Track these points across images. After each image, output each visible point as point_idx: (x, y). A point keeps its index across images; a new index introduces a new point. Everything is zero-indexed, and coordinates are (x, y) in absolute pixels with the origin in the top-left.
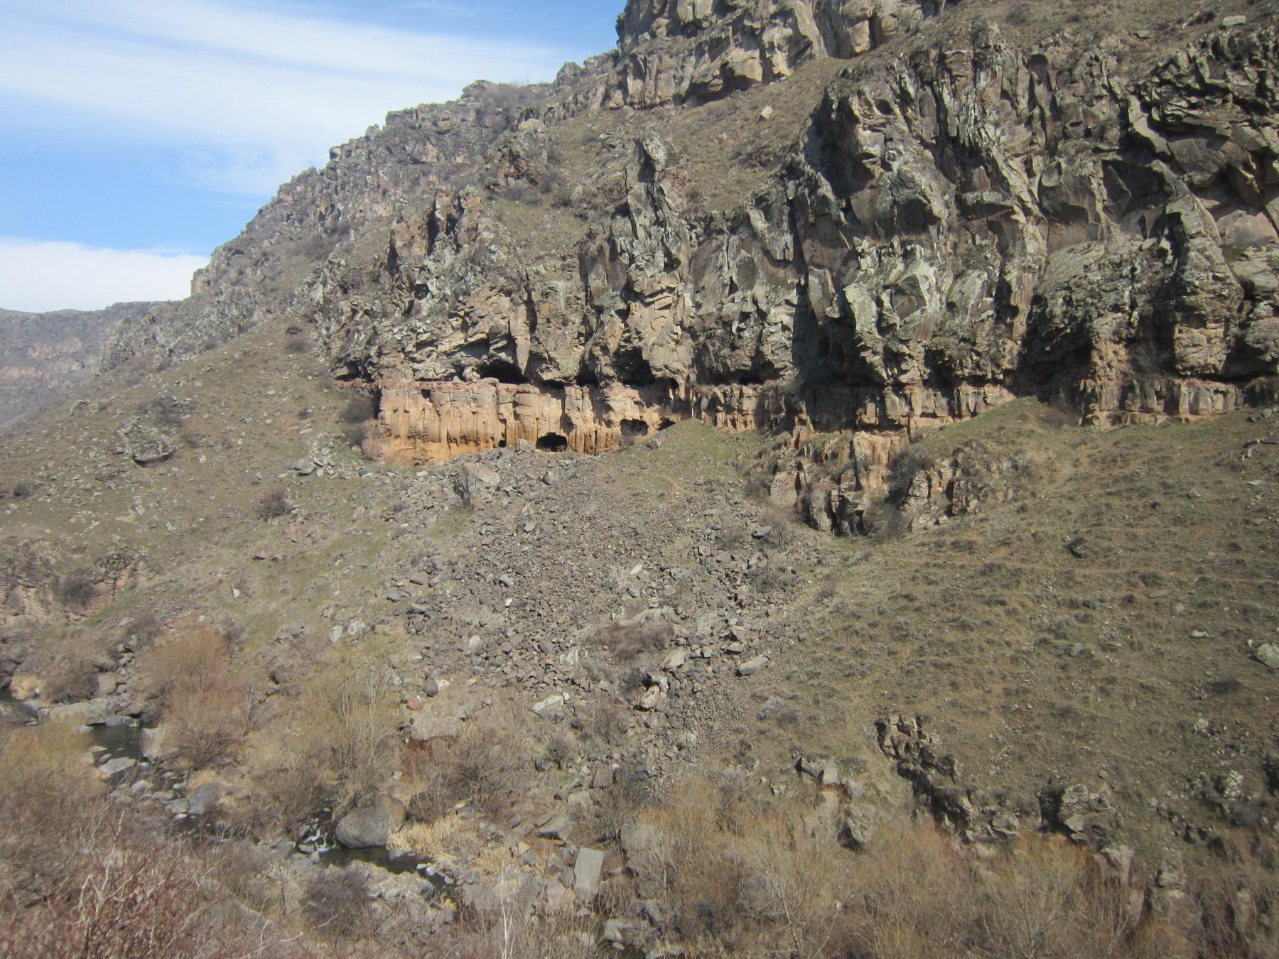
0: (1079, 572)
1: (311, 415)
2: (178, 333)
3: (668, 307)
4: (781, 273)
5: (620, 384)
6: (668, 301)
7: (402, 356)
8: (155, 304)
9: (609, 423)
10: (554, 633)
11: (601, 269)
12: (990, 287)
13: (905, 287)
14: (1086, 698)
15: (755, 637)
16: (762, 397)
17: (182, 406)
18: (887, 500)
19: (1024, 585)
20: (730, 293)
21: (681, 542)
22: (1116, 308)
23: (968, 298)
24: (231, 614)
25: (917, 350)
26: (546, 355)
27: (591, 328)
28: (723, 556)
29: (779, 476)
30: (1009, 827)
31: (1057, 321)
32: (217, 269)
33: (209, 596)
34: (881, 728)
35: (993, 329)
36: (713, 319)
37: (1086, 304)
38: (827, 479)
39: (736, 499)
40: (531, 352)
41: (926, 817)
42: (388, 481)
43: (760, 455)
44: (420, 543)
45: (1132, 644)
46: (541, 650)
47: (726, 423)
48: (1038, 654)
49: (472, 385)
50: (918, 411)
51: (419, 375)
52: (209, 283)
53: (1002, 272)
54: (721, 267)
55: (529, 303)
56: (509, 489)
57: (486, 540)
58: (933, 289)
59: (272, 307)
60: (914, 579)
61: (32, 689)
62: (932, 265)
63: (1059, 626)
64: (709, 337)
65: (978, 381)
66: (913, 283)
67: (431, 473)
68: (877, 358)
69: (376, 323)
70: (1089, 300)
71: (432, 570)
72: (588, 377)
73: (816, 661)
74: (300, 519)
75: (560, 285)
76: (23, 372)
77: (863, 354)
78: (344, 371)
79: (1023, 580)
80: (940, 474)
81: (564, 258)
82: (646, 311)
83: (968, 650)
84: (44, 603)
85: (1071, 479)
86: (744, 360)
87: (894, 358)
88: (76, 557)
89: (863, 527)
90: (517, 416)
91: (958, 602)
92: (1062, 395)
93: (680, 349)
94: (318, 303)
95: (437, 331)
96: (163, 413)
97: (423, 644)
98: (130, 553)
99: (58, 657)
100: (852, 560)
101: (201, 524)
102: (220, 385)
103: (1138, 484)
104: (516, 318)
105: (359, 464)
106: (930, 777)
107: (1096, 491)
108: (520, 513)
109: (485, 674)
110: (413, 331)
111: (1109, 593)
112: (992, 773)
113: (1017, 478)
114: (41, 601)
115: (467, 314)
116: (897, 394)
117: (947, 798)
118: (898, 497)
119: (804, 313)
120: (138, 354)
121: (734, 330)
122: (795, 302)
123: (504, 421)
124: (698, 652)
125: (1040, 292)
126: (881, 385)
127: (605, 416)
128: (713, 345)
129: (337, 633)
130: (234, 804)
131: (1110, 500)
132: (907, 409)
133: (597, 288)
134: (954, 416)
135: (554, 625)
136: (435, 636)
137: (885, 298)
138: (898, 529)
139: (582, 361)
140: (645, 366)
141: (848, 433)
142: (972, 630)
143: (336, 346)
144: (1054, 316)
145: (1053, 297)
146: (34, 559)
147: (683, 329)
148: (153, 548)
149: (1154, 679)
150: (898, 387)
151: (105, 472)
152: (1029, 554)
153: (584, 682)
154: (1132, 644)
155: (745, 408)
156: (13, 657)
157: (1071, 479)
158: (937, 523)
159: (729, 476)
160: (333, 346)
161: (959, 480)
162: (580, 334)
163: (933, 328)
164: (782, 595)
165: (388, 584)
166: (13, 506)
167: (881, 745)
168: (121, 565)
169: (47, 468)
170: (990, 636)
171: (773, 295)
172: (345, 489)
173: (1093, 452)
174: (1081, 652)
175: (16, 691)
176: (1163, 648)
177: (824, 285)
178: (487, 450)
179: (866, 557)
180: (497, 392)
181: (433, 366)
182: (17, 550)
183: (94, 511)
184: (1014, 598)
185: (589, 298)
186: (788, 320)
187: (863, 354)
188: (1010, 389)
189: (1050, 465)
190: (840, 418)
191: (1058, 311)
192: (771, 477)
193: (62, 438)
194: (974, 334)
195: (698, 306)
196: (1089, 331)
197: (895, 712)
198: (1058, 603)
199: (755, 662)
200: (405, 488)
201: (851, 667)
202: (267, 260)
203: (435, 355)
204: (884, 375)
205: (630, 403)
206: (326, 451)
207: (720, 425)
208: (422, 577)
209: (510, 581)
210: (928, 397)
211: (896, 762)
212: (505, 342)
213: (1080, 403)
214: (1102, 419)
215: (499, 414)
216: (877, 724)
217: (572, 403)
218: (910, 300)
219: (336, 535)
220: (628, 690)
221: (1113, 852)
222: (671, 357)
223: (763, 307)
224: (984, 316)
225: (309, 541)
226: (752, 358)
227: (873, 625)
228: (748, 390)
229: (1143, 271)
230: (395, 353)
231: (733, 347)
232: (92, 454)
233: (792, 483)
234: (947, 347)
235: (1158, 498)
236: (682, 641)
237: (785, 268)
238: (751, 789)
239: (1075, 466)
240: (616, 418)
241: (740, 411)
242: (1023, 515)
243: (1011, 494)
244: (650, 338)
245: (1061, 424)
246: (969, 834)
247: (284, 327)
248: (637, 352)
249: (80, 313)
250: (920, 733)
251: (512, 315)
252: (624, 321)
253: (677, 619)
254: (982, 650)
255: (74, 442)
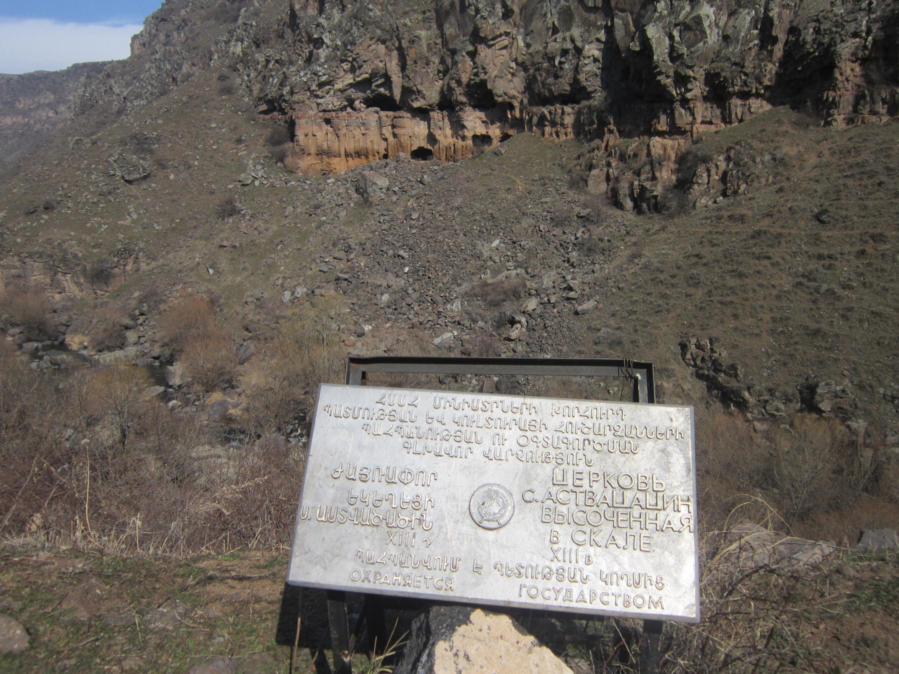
0: (824, 234)
1: (244, 141)
2: (128, 84)
3: (505, 47)
4: (592, 17)
5: (471, 108)
6: (506, 42)
7: (309, 94)
8: (110, 62)
9: (464, 138)
10: (441, 290)
11: (453, 20)
12: (757, 21)
13: (692, 24)
14: (832, 322)
15: (586, 288)
16: (578, 114)
17: (151, 139)
18: (675, 187)
19: (783, 244)
20: (553, 35)
21: (526, 222)
22: (855, 35)
23: (740, 31)
24: (210, 286)
25: (699, 73)
26: (415, 88)
27: (447, 66)
28: (557, 231)
29: (595, 172)
30: (778, 410)
31: (808, 46)
32: (150, 33)
33: (192, 274)
34: (684, 347)
35: (758, 55)
36: (540, 55)
37: (831, 32)
38: (630, 173)
39: (563, 190)
40: (403, 87)
41: (718, 406)
42: (307, 187)
43: (579, 157)
44: (337, 230)
45: (864, 284)
46: (433, 302)
47: (551, 134)
48: (796, 293)
49: (361, 114)
50: (699, 120)
51: (321, 108)
52: (144, 45)
53: (767, 9)
54: (545, 14)
55: (400, 49)
56: (396, 189)
57: (384, 227)
58: (713, 25)
59: (196, 62)
60: (701, 243)
61: (81, 343)
62: (712, 6)
63: (811, 273)
64: (538, 69)
65: (745, 96)
66: (698, 20)
67: (337, 180)
68: (669, 80)
69: (285, 69)
70: (834, 29)
71: (348, 250)
72: (447, 104)
73: (634, 303)
74: (248, 217)
75: (423, 33)
76: (15, 119)
77: (659, 78)
78: (264, 107)
79: (783, 241)
80: (717, 166)
81: (424, 13)
82: (489, 52)
83: (745, 291)
84: (78, 284)
85: (816, 167)
86: (564, 85)
87: (682, 80)
88: (95, 251)
89: (657, 207)
90: (395, 135)
91: (735, 259)
92: (809, 104)
93: (516, 80)
94: (239, 55)
95: (333, 74)
96: (138, 144)
97: (349, 301)
98: (132, 246)
99: (95, 321)
100: (653, 231)
101: (178, 224)
102: (175, 122)
103: (868, 169)
104: (391, 61)
105: (284, 176)
106: (720, 379)
107: (835, 175)
108: (406, 206)
109: (396, 320)
110: (315, 74)
111: (847, 248)
112: (765, 374)
113: (776, 167)
114: (76, 283)
115: (354, 59)
116: (683, 107)
117: (733, 392)
118: (684, 184)
119: (610, 48)
120: (100, 102)
121: (557, 63)
122: (603, 39)
123: (386, 140)
124: (546, 299)
125: (795, 24)
126: (671, 100)
127: (460, 133)
128: (541, 76)
129: (287, 296)
130: (239, 413)
131: (847, 181)
132: (690, 119)
133: (451, 35)
134: (725, 122)
135: (441, 285)
136: (357, 296)
137: (676, 33)
138: (685, 208)
139: (442, 92)
140: (490, 94)
141: (646, 138)
142: (746, 277)
143: (256, 88)
144: (806, 43)
145: (805, 28)
146: (67, 254)
147: (517, 64)
148: (147, 242)
149: (881, 307)
150: (685, 102)
151: (105, 189)
152: (786, 222)
153: (467, 323)
154: (864, 284)
155: (566, 122)
156: (64, 322)
157: (816, 167)
158: (715, 202)
159: (556, 174)
160: (254, 88)
161: (731, 170)
162: (439, 72)
163: (712, 56)
164: (602, 258)
165: (318, 261)
166: (45, 216)
167: (683, 359)
168: (127, 255)
169: (63, 188)
170: (760, 281)
171: (587, 35)
172: (276, 195)
173: (832, 146)
174: (827, 291)
175: (70, 345)
176: (887, 286)
177: (626, 25)
178: (375, 161)
179: (663, 229)
180: (380, 118)
181: (331, 101)
182: (54, 248)
183: (102, 218)
184: (776, 254)
185: (445, 43)
186: (597, 53)
187: (659, 78)
188: (769, 100)
189: (800, 157)
190: (639, 127)
191: (809, 39)
192: (587, 173)
193: (69, 166)
194: (743, 59)
195: (528, 46)
196: (834, 53)
197: (693, 336)
198: (809, 256)
199: (588, 305)
200: (320, 191)
201: (659, 306)
202: (186, 25)
203: (332, 92)
204: (674, 93)
205: (479, 122)
206: (259, 167)
207: (547, 136)
208: (342, 255)
209: (406, 255)
210: (706, 109)
211: (694, 369)
212: (383, 80)
213: (822, 110)
214: (839, 120)
215: (382, 134)
216: (680, 344)
217: (436, 125)
218: (695, 34)
219: (275, 227)
220: (498, 327)
221: (854, 425)
222: (509, 87)
223: (579, 44)
224: (751, 45)
225: (256, 232)
226: (570, 85)
227: (673, 276)
228: (568, 109)
229: (878, 5)
230: (302, 92)
231: (556, 77)
232: (93, 177)
233: (603, 177)
234: (722, 70)
235: (883, 178)
236: (533, 292)
237: (595, 13)
238: (594, 391)
239: (819, 156)
240: (469, 134)
241: (562, 125)
242: (781, 194)
243: (771, 179)
244: (493, 72)
245: (808, 125)
246: (749, 415)
247: (215, 76)
248: (483, 83)
249: (49, 73)
250: (712, 349)
251: (387, 59)
252: (473, 60)
253: (528, 277)
254: (754, 291)
255: (79, 169)
